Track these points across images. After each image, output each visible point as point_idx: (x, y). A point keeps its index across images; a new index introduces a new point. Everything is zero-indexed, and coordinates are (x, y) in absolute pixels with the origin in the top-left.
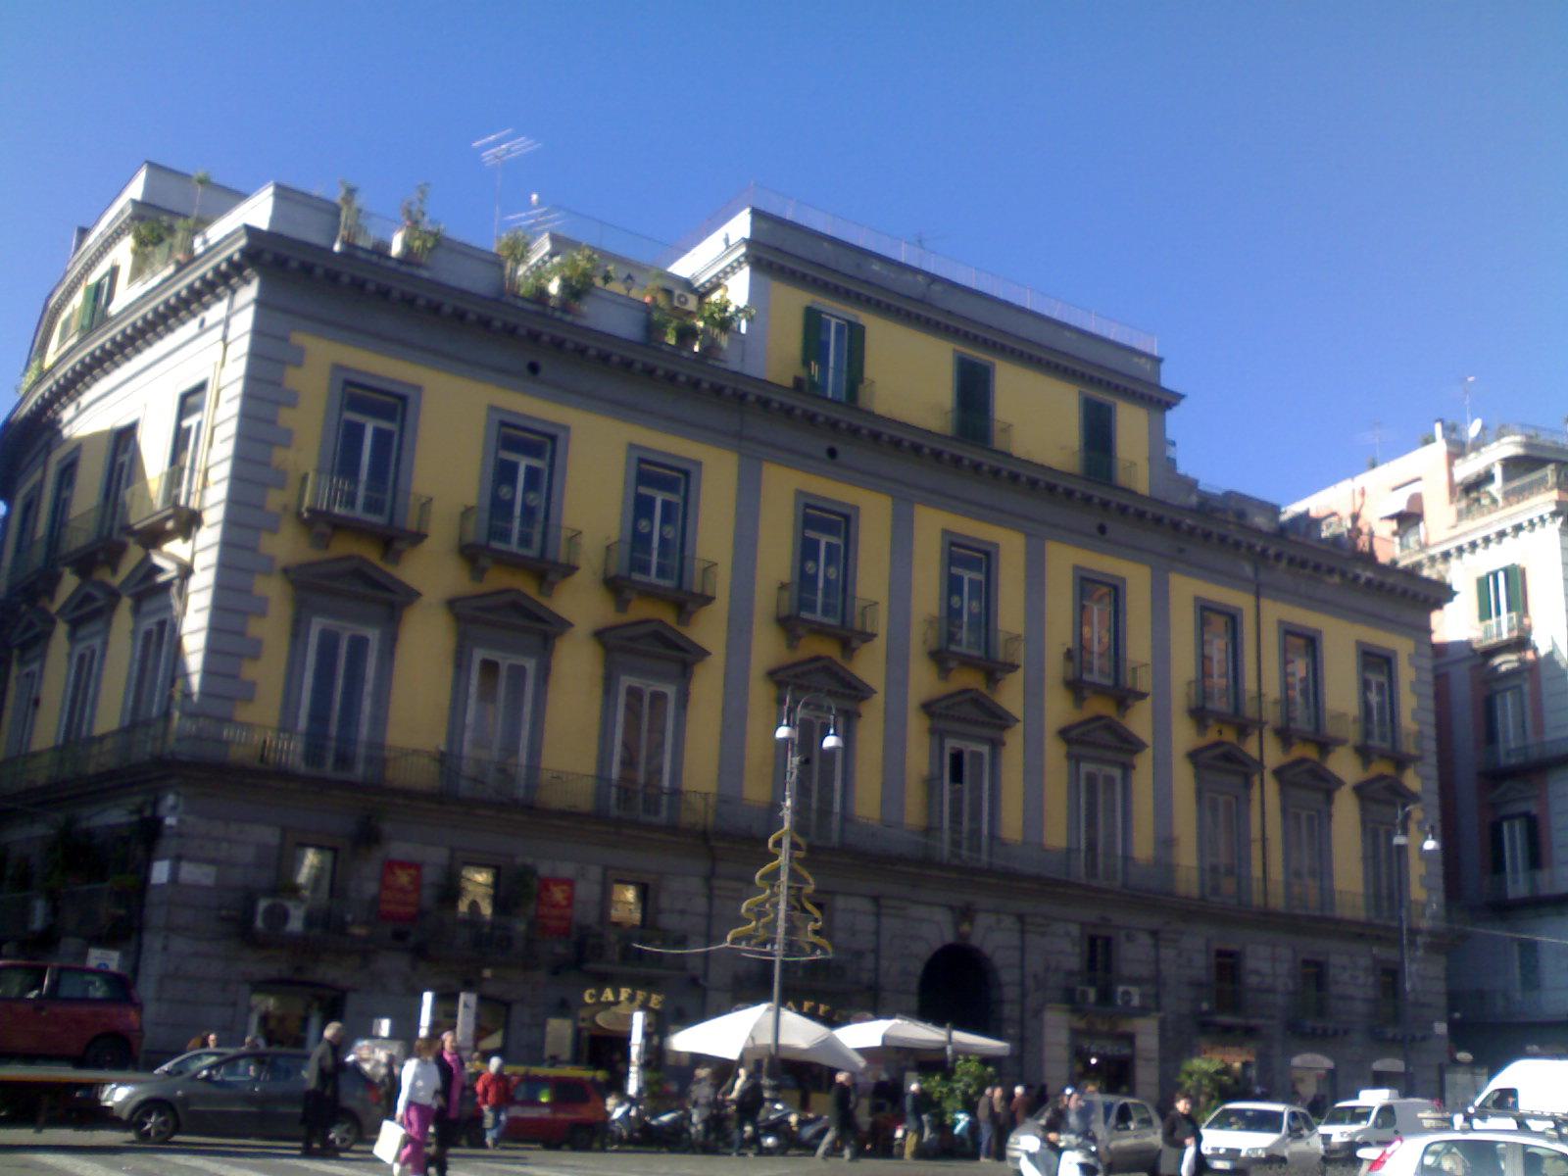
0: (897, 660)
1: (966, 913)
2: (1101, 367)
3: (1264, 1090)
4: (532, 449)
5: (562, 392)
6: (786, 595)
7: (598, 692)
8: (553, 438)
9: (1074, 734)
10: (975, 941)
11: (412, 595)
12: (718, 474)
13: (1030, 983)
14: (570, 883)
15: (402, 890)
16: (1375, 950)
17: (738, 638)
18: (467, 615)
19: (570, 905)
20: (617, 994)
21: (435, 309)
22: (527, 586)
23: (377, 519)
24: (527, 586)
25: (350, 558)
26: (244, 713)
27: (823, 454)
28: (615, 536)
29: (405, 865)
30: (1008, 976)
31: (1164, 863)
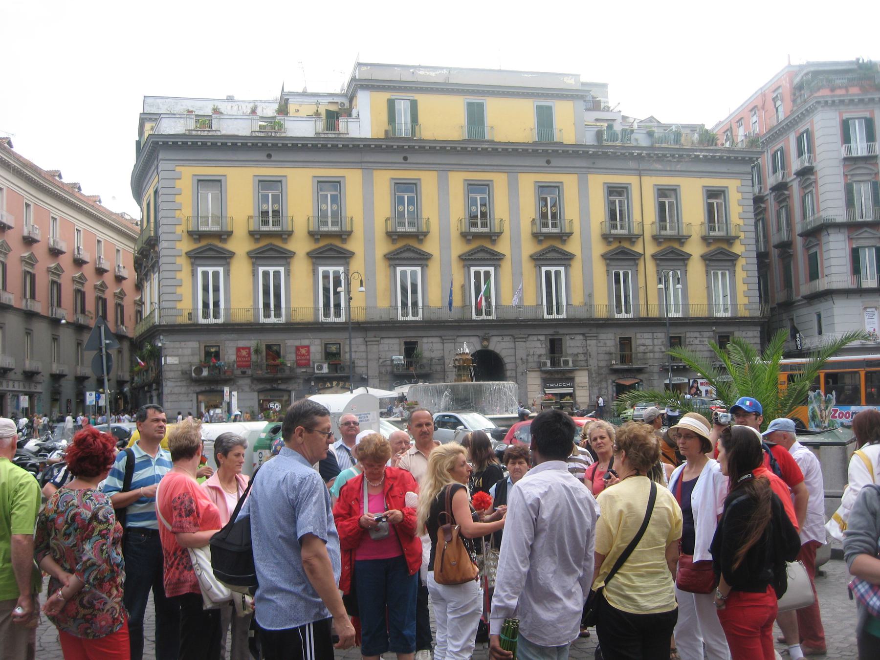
0: (369, 242)
1: (486, 338)
2: (391, 81)
3: (129, 394)
4: (620, 194)
5: (282, 163)
6: (654, 226)
7: (311, 275)
8: (626, 188)
9: (192, 254)
10: (491, 347)
11: (232, 255)
12: (569, 182)
13: (519, 362)
14: (308, 347)
15: (244, 357)
16: (714, 328)
17: (368, 247)
18: (707, 259)
19: (309, 355)
20: (332, 384)
21: (224, 145)
22: (725, 246)
23: (336, 229)
24: (725, 246)
25: (327, 245)
26: (179, 306)
27: (265, 158)
28: (462, 217)
29: (244, 348)
30: (507, 360)
31: (589, 304)
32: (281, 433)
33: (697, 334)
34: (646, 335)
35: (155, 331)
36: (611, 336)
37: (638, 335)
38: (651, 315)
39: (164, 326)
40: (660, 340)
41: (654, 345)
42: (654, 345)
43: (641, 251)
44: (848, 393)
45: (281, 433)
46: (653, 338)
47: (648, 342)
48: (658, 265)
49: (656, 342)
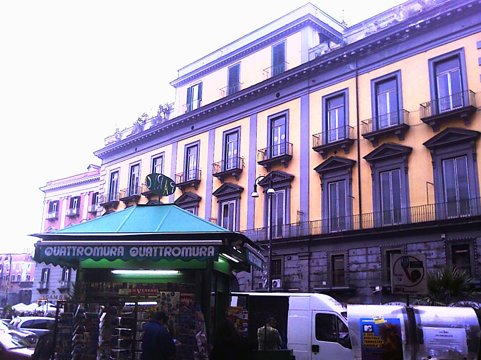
16: (443, 236)
27: (79, 223)
32: (123, 309)
33: (421, 246)
34: (359, 252)
35: (246, 248)
36: (323, 254)
37: (351, 252)
38: (365, 226)
39: (294, 238)
40: (375, 257)
41: (368, 262)
42: (368, 262)
43: (355, 158)
44: (8, 311)
45: (123, 309)
46: (367, 255)
47: (361, 259)
48: (372, 168)
49: (370, 258)
